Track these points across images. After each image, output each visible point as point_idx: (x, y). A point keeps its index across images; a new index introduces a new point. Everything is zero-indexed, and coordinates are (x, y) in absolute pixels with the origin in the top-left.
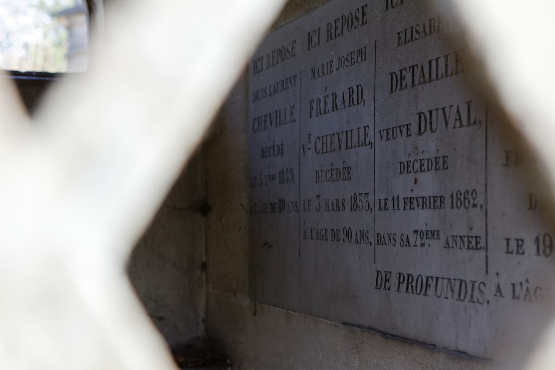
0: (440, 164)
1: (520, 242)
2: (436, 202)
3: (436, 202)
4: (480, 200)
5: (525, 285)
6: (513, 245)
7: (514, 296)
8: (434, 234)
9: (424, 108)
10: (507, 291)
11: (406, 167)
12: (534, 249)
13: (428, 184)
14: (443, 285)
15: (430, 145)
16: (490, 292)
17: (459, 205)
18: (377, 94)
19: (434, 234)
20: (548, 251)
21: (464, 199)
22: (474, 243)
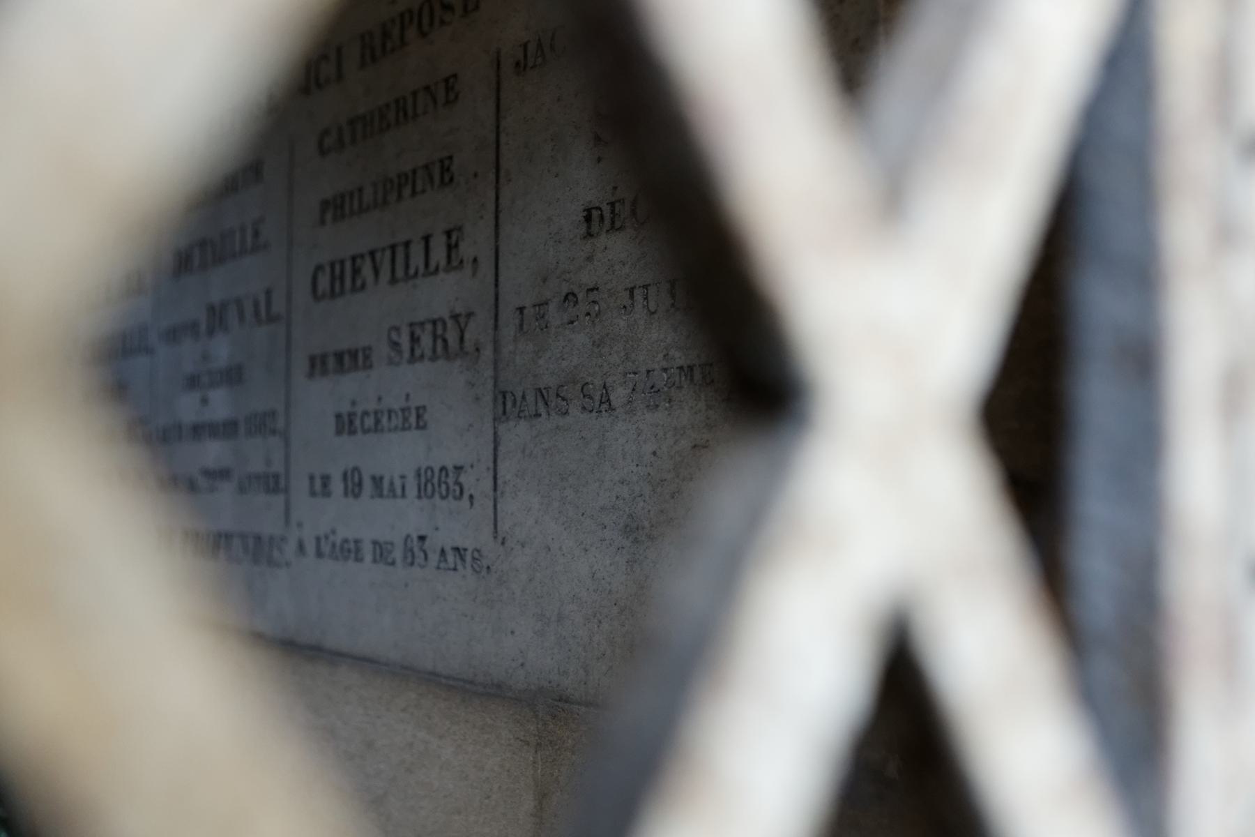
0: (233, 376)
1: (326, 480)
2: (228, 429)
3: (228, 429)
4: (280, 424)
5: (332, 538)
6: (318, 483)
7: (319, 554)
8: (224, 474)
9: (216, 297)
10: (310, 548)
11: (193, 382)
12: (415, 492)
13: (221, 405)
14: (236, 542)
15: (222, 350)
16: (291, 547)
17: (429, 473)
18: (503, 467)
19: (224, 474)
20: (356, 490)
21: (262, 424)
22: (273, 483)
